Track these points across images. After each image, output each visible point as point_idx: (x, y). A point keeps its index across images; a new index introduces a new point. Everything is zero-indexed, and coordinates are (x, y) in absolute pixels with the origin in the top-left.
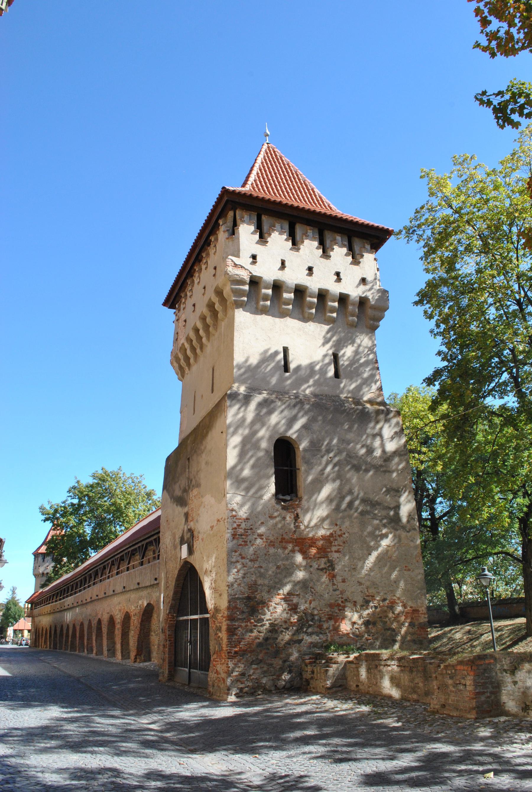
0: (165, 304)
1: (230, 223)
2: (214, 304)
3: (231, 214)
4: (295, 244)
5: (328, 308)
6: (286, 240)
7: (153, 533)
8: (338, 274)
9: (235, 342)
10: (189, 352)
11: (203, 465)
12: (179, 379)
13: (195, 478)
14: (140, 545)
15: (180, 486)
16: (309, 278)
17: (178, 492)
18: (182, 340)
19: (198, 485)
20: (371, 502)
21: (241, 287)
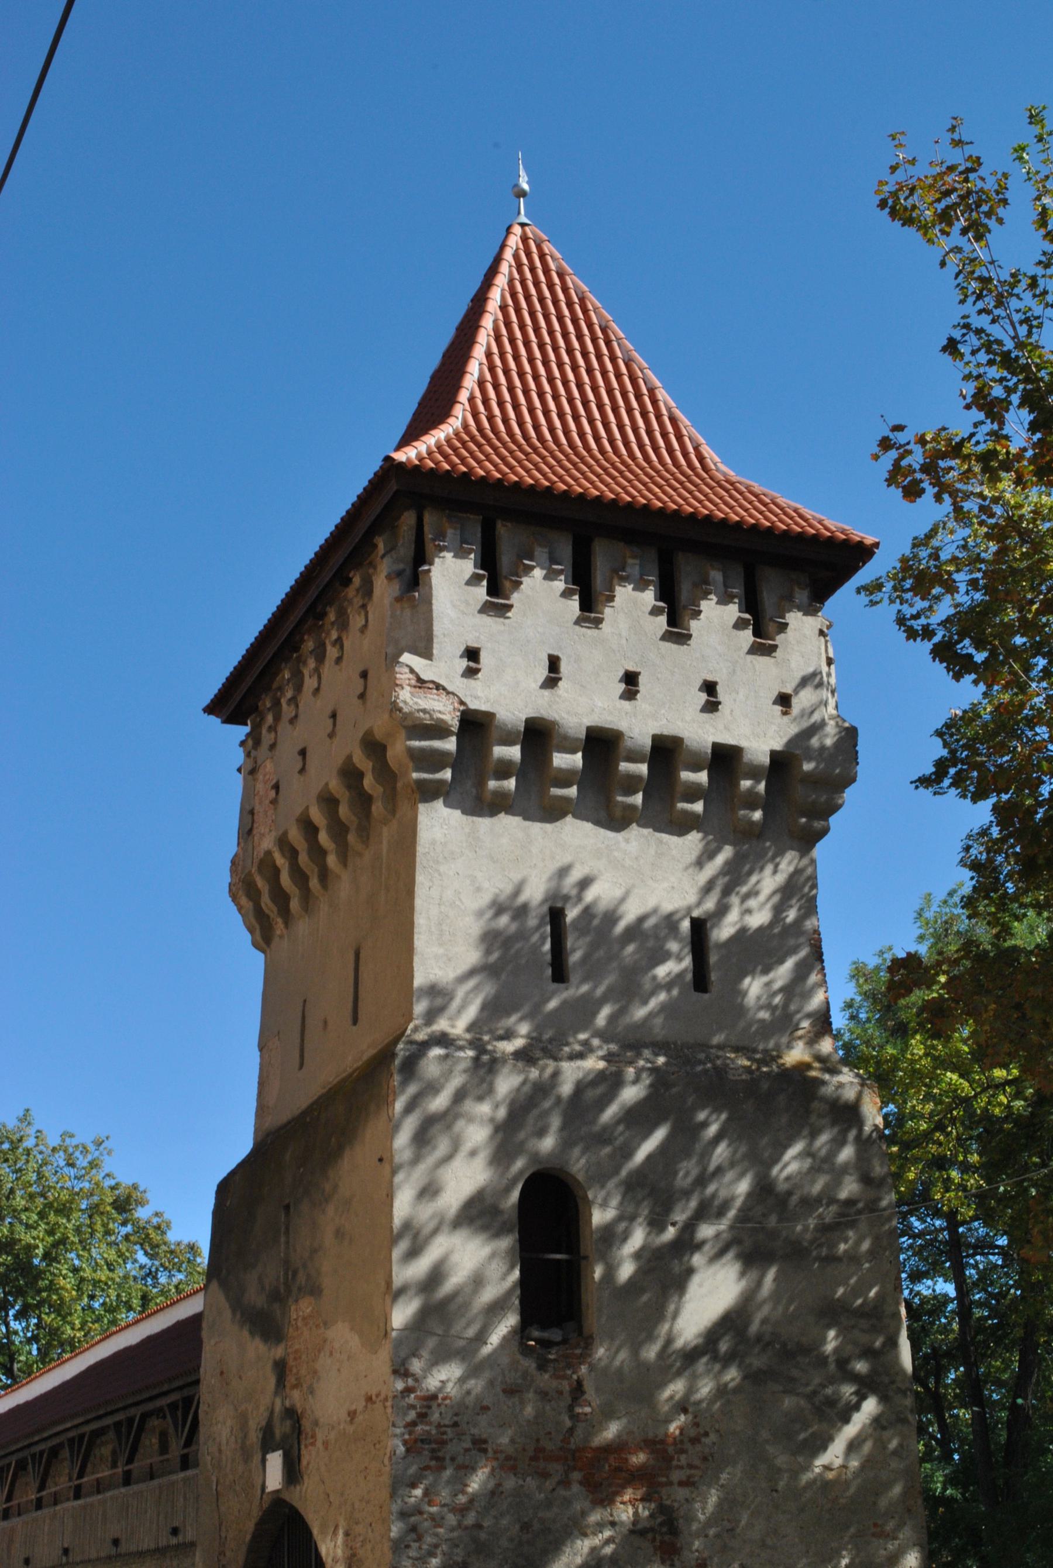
0: (211, 709)
1: (405, 549)
2: (361, 775)
3: (408, 520)
4: (591, 603)
5: (679, 789)
6: (566, 594)
7: (166, 1388)
8: (710, 688)
9: (418, 902)
10: (285, 880)
11: (328, 1238)
12: (255, 945)
13: (305, 1265)
14: (119, 1417)
15: (260, 1279)
16: (626, 705)
17: (255, 1297)
18: (267, 843)
19: (315, 1291)
20: (784, 1345)
21: (437, 744)
